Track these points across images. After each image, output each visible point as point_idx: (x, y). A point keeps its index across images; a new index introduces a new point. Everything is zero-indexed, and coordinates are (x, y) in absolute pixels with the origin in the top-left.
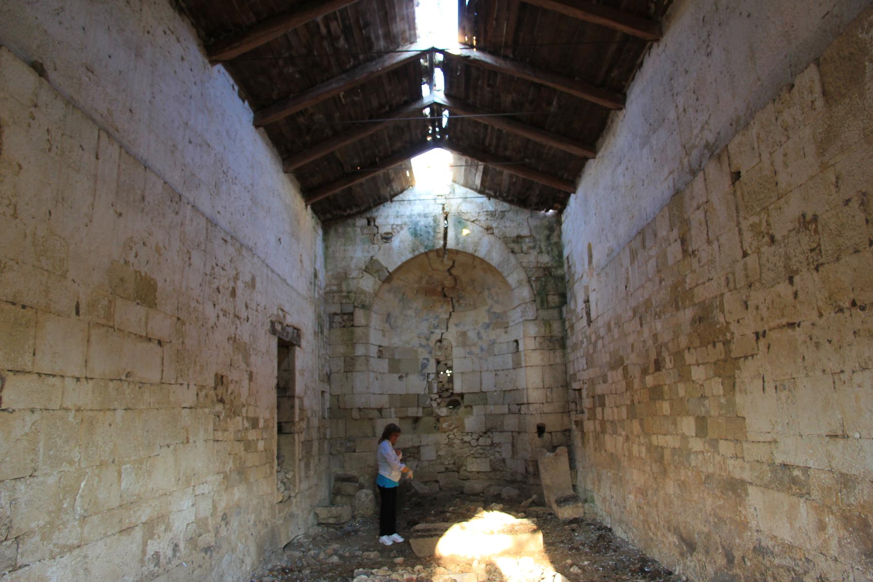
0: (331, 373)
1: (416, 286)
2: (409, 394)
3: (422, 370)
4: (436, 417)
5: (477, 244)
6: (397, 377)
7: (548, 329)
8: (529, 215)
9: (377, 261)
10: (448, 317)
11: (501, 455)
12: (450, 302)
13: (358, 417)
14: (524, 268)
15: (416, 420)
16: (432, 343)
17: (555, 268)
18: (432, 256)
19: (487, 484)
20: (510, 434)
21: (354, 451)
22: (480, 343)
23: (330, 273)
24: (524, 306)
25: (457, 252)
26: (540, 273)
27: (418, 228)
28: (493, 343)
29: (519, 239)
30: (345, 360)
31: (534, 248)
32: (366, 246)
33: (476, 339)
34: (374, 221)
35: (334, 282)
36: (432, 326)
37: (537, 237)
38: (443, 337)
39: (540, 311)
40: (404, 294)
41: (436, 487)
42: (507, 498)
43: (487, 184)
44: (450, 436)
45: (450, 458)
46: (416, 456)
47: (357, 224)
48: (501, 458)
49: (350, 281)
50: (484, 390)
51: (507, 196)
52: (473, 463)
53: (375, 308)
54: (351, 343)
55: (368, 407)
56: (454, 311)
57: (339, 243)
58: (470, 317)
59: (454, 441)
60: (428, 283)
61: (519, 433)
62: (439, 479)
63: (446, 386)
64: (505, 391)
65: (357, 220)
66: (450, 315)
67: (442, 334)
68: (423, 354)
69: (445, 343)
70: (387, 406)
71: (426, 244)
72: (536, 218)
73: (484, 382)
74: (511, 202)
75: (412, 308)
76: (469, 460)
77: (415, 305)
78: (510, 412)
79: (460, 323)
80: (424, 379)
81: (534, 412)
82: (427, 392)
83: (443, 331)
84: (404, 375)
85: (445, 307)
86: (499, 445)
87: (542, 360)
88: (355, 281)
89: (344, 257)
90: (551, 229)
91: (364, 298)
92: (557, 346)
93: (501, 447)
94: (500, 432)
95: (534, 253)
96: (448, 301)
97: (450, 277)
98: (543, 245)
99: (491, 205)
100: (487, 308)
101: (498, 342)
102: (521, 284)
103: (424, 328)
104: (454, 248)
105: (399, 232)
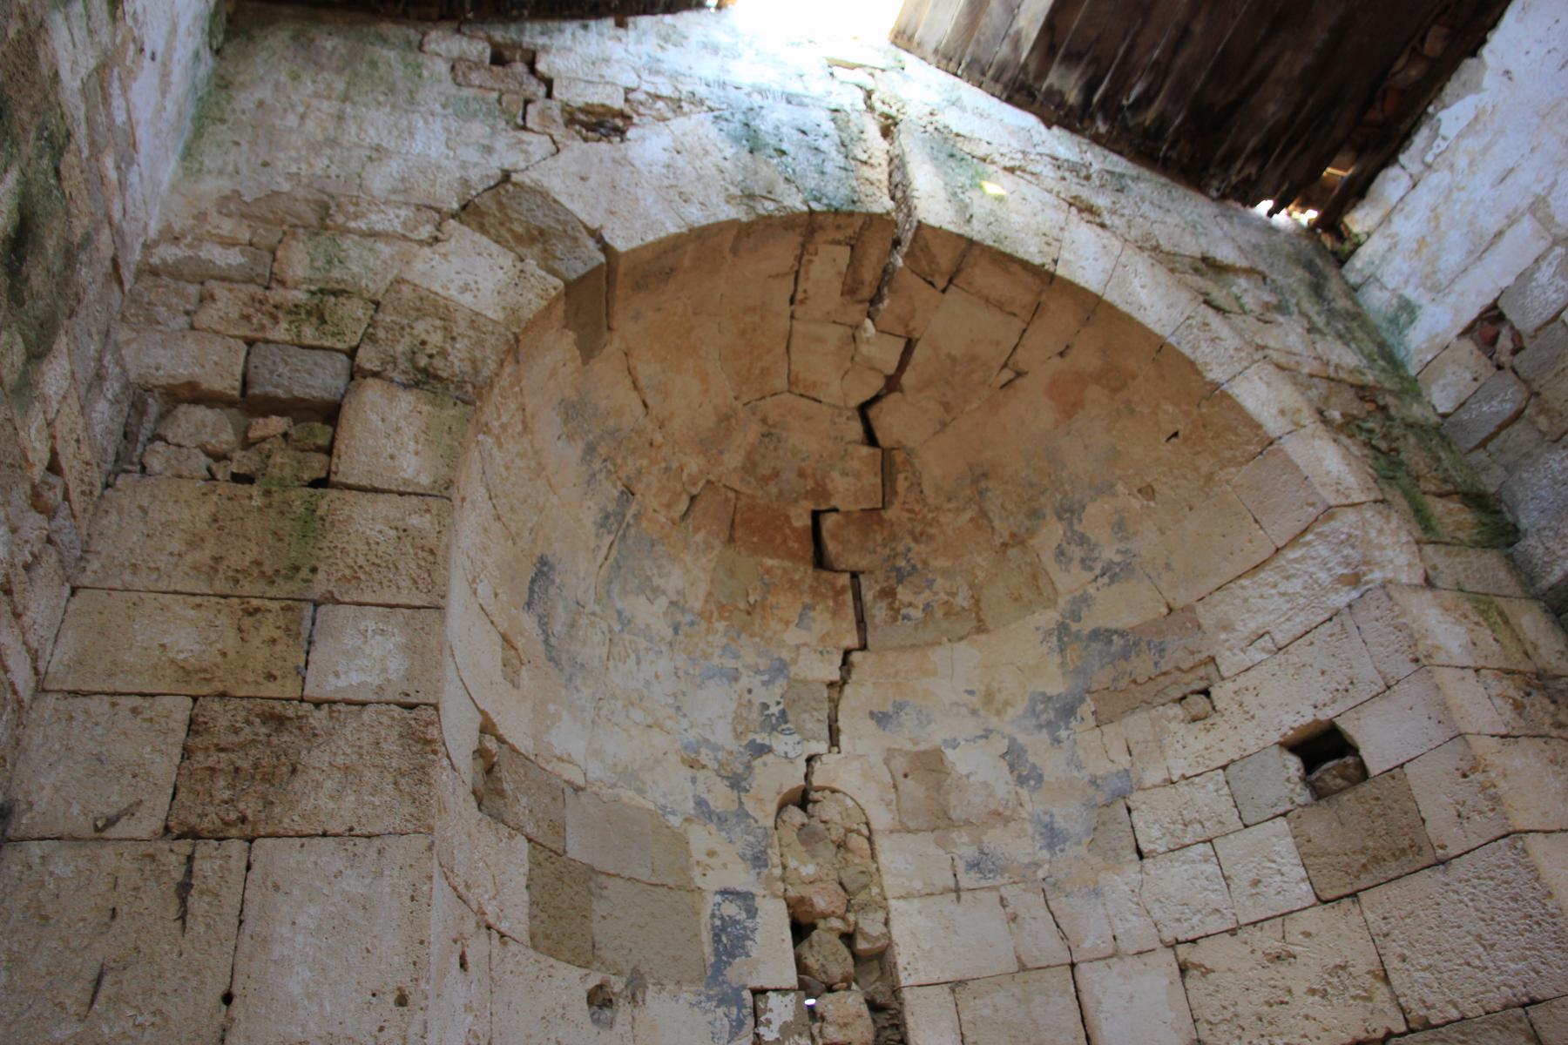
1: (694, 464)
3: (719, 967)
9: (542, 194)
10: (835, 676)
12: (849, 597)
18: (828, 264)
22: (1033, 804)
30: (193, 726)
32: (478, 130)
33: (1002, 783)
38: (817, 780)
40: (629, 492)
47: (431, 47)
56: (863, 647)
57: (309, 87)
60: (750, 466)
69: (828, 809)
71: (811, 183)
75: (657, 591)
77: (674, 581)
79: (899, 707)
84: (618, 985)
85: (821, 621)
88: (385, 249)
96: (838, 593)
97: (865, 451)
100: (1048, 618)
101: (1154, 776)
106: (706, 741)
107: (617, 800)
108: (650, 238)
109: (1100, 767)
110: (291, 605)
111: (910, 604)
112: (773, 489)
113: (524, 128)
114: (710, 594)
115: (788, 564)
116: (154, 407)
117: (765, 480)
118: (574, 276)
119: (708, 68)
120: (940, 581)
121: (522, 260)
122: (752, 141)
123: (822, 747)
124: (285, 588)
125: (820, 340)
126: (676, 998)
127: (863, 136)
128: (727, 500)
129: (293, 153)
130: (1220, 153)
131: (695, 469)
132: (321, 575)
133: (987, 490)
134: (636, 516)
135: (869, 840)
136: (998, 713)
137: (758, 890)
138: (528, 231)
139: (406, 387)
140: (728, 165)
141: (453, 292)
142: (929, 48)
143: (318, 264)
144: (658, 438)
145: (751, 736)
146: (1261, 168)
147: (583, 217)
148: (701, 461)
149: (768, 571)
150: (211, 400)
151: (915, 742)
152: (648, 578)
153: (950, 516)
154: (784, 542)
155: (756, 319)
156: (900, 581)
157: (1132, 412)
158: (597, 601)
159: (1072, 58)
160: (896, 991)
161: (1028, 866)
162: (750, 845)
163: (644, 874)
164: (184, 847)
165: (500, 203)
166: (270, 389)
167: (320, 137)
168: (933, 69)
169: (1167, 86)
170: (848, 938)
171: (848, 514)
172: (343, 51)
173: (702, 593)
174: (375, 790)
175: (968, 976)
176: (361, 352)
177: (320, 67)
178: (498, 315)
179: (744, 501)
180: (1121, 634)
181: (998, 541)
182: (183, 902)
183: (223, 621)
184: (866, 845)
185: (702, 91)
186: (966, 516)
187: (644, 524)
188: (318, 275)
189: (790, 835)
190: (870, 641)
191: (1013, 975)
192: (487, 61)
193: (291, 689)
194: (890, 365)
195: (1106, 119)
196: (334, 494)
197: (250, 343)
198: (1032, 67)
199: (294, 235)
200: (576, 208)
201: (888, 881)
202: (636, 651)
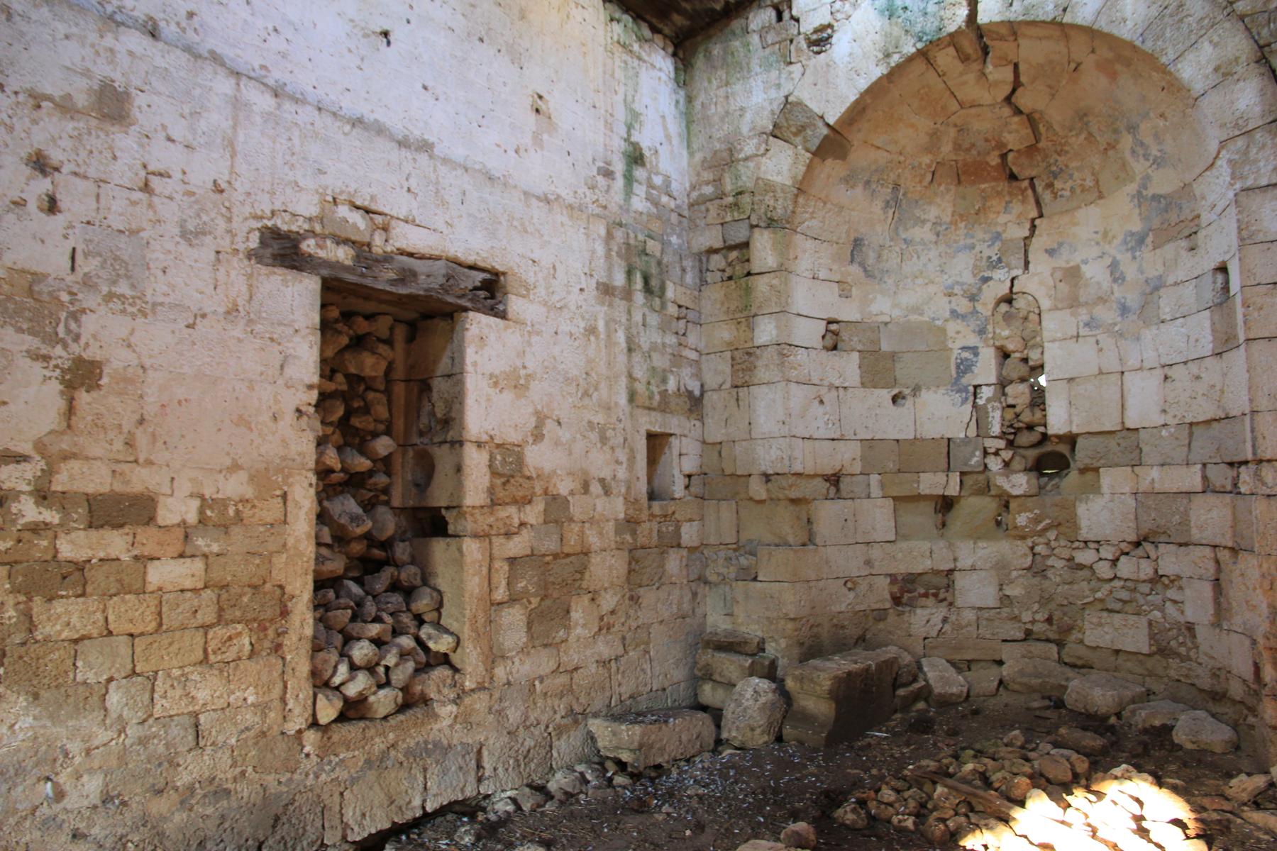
0: (703, 393)
1: (926, 159)
2: (923, 440)
4: (999, 496)
9: (799, 104)
10: (1027, 233)
11: (1182, 612)
12: (1030, 192)
13: (764, 496)
14: (1242, 18)
15: (946, 504)
16: (985, 307)
18: (946, 58)
20: (1208, 552)
21: (755, 579)
22: (1118, 292)
23: (699, 157)
24: (1240, 143)
25: (1013, 29)
30: (733, 359)
32: (774, 74)
35: (708, 176)
36: (984, 263)
38: (1015, 290)
40: (896, 187)
41: (986, 679)
44: (1038, 549)
45: (1036, 606)
47: (752, 26)
48: (1182, 620)
49: (741, 167)
50: (1130, 424)
52: (1100, 625)
54: (746, 316)
56: (1041, 216)
59: (1049, 562)
60: (957, 147)
61: (1234, 551)
62: (1004, 658)
63: (1027, 417)
64: (1191, 424)
65: (751, 16)
66: (1033, 227)
67: (1013, 280)
68: (961, 336)
69: (1020, 303)
70: (857, 468)
71: (918, 28)
73: (1130, 402)
75: (924, 222)
76: (1092, 617)
77: (932, 213)
79: (1061, 245)
80: (965, 401)
82: (972, 432)
83: (1014, 273)
84: (907, 391)
85: (1017, 207)
86: (1175, 580)
88: (751, 164)
89: (727, 113)
91: (771, 203)
93: (1181, 588)
94: (1180, 545)
96: (1023, 191)
97: (1016, 119)
100: (1132, 188)
101: (1171, 280)
103: (962, 269)
104: (997, 19)
105: (848, 18)
111: (1063, 189)
112: (974, 152)
114: (954, 212)
115: (993, 184)
116: (704, 259)
117: (968, 150)
124: (746, 313)
125: (965, 83)
126: (936, 392)
128: (951, 166)
131: (928, 161)
133: (1089, 122)
134: (904, 195)
135: (1039, 314)
136: (1110, 243)
137: (980, 345)
139: (766, 228)
144: (902, 159)
145: (982, 274)
147: (816, 110)
148: (930, 156)
149: (983, 191)
150: (716, 251)
151: (1067, 262)
152: (919, 218)
153: (1074, 139)
154: (989, 174)
155: (927, 90)
156: (1055, 178)
157: (1141, 76)
158: (892, 240)
161: (1111, 325)
162: (978, 325)
170: (1025, 360)
171: (1018, 151)
173: (949, 214)
175: (1076, 376)
180: (1165, 198)
181: (1102, 148)
183: (733, 327)
184: (1036, 318)
186: (1083, 137)
187: (909, 195)
189: (999, 318)
190: (1044, 212)
191: (1096, 376)
197: (722, 224)
201: (1046, 334)
202: (917, 253)
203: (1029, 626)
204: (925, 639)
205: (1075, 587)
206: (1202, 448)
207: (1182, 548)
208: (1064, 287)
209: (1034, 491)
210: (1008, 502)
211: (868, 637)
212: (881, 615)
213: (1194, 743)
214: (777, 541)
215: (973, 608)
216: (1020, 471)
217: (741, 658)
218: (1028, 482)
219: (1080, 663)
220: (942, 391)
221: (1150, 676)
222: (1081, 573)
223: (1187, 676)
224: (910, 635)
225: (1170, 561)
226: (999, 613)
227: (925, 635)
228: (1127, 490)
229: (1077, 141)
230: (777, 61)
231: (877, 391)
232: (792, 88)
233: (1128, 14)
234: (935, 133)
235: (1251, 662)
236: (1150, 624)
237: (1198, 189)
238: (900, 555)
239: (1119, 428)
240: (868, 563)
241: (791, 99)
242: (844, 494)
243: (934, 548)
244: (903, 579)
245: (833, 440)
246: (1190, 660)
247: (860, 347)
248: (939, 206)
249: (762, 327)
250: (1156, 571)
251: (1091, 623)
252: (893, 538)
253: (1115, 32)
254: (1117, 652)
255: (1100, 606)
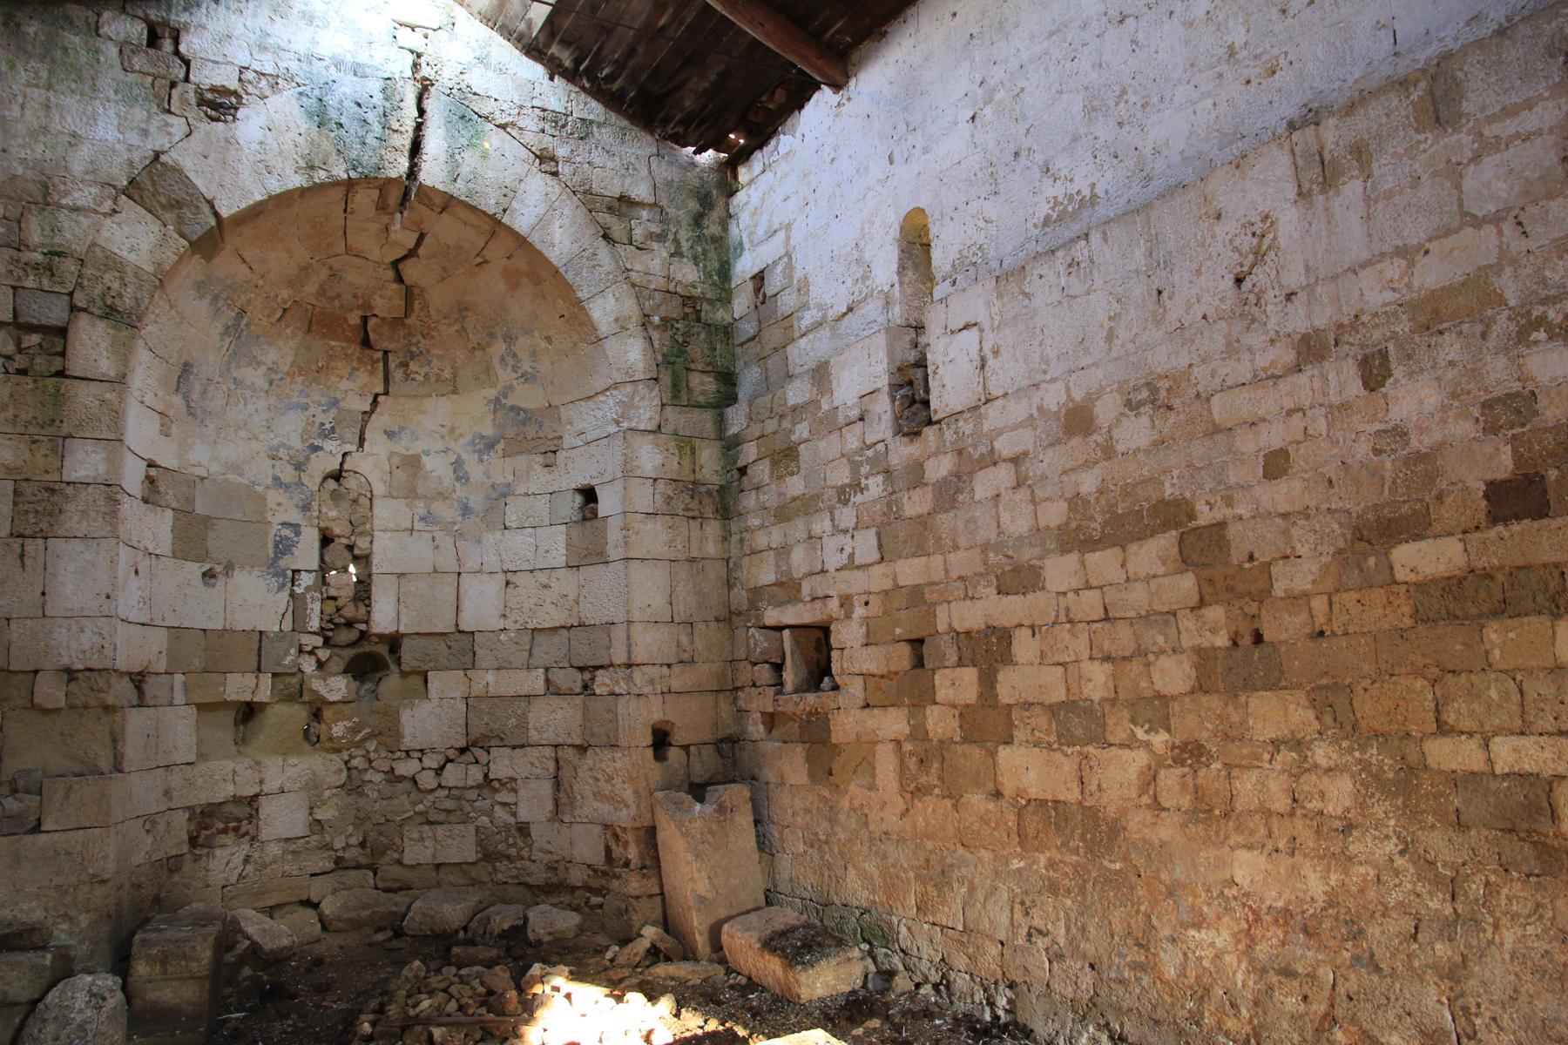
1: (285, 293)
2: (233, 631)
5: (509, 193)
6: (199, 573)
7: (686, 463)
8: (655, 151)
9: (177, 170)
10: (367, 408)
11: (514, 814)
12: (381, 365)
14: (634, 285)
15: (249, 712)
16: (312, 480)
17: (711, 302)
18: (365, 199)
19: (473, 899)
21: (37, 829)
22: (461, 492)
24: (629, 388)
25: (447, 203)
26: (673, 309)
27: (331, 101)
28: (503, 494)
29: (624, 205)
31: (661, 237)
32: (139, 114)
34: (176, 42)
36: (315, 429)
37: (672, 211)
38: (346, 467)
39: (669, 409)
42: (547, 938)
43: (567, 23)
44: (355, 763)
46: (244, 827)
48: (512, 820)
51: (611, 78)
53: (150, 329)
55: (108, 664)
56: (386, 393)
57: (23, 76)
58: (437, 412)
59: (367, 777)
60: (322, 291)
61: (582, 749)
63: (349, 612)
66: (375, 402)
68: (282, 509)
69: (350, 482)
71: (354, 154)
72: (670, 163)
73: (466, 605)
74: (612, 101)
75: (259, 363)
77: (271, 356)
78: (551, 689)
79: (402, 429)
80: (281, 587)
81: (645, 690)
82: (287, 625)
83: (348, 448)
84: (219, 569)
85: (362, 377)
86: (510, 784)
87: (671, 543)
88: (85, 221)
89: (45, 129)
90: (706, 201)
92: (709, 510)
94: (514, 748)
95: (661, 252)
96: (375, 362)
97: (395, 286)
98: (684, 235)
99: (557, 95)
100: (491, 393)
101: (521, 490)
102: (624, 328)
103: (291, 430)
104: (441, 187)
105: (264, 97)
106: (284, 445)
107: (226, 480)
108: (243, 206)
109: (499, 479)
110: (53, 438)
112: (337, 303)
113: (169, 112)
117: (332, 299)
118: (195, 237)
119: (301, 44)
120: (435, 362)
121: (165, 226)
122: (320, 117)
123: (353, 448)
124: (49, 430)
125: (365, 230)
127: (402, 105)
128: (307, 310)
129: (20, 141)
130: (661, 115)
132: (65, 424)
138: (169, 200)
139: (101, 317)
140: (301, 140)
141: (125, 254)
142: (475, 10)
143: (46, 233)
144: (261, 283)
146: (686, 129)
147: (203, 190)
148: (290, 291)
149: (332, 348)
153: (445, 327)
156: (412, 359)
157: (544, 297)
159: (565, 43)
160: (370, 575)
163: (238, 516)
164: (20, 540)
165: (152, 180)
166: (30, 320)
167: (36, 127)
168: (477, 22)
169: (624, 73)
171: (383, 319)
172: (43, 38)
173: (289, 364)
174: (95, 520)
176: (75, 295)
177: (30, 56)
178: (150, 269)
179: (318, 310)
180: (525, 411)
182: (22, 561)
184: (368, 502)
185: (294, 66)
186: (454, 328)
187: (252, 327)
188: (47, 241)
189: (326, 495)
192: (145, 42)
193: (56, 477)
194: (411, 245)
195: (588, 81)
196: (67, 381)
198: (541, 39)
199: (29, 209)
200: (199, 182)
201: (376, 522)
202: (244, 399)
203: (340, 854)
204: (223, 887)
205: (395, 802)
206: (547, 653)
207: (517, 751)
208: (400, 475)
209: (352, 697)
210: (319, 710)
211: (163, 895)
212: (173, 865)
213: (550, 934)
214: (77, 768)
215: (279, 840)
216: (337, 674)
217: (31, 954)
218: (347, 686)
219: (396, 886)
220: (257, 572)
221: (473, 885)
222: (400, 786)
223: (516, 877)
224: (208, 886)
225: (502, 764)
226: (308, 843)
227: (224, 882)
228: (458, 694)
229: (447, 330)
230: (146, 99)
231: (189, 564)
232: (167, 145)
233: (556, 241)
234: (306, 268)
235: (602, 848)
236: (477, 830)
237: (564, 413)
238: (200, 780)
239: (452, 629)
240: (167, 793)
241: (163, 158)
242: (148, 700)
243: (237, 769)
244: (202, 812)
245: (143, 625)
246: (522, 858)
247: (174, 505)
248: (280, 350)
249: (80, 456)
250: (486, 776)
251: (411, 839)
252: (192, 758)
253: (545, 252)
254: (438, 866)
255: (419, 820)
